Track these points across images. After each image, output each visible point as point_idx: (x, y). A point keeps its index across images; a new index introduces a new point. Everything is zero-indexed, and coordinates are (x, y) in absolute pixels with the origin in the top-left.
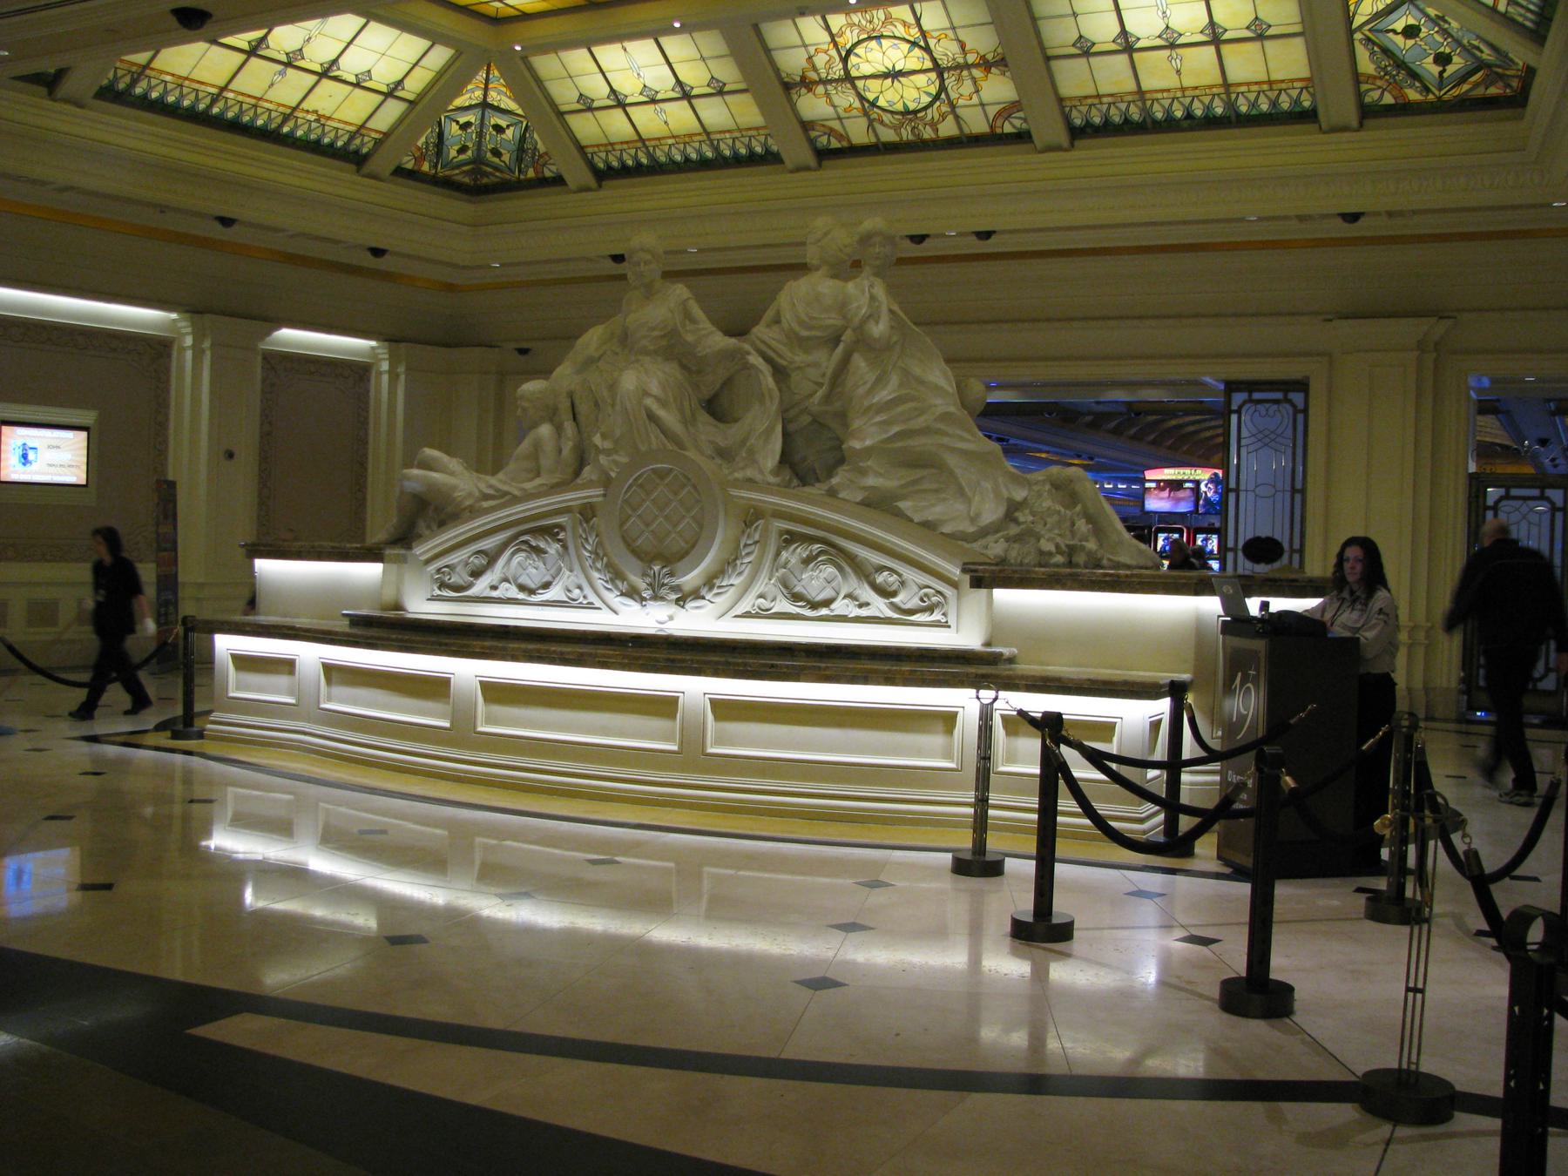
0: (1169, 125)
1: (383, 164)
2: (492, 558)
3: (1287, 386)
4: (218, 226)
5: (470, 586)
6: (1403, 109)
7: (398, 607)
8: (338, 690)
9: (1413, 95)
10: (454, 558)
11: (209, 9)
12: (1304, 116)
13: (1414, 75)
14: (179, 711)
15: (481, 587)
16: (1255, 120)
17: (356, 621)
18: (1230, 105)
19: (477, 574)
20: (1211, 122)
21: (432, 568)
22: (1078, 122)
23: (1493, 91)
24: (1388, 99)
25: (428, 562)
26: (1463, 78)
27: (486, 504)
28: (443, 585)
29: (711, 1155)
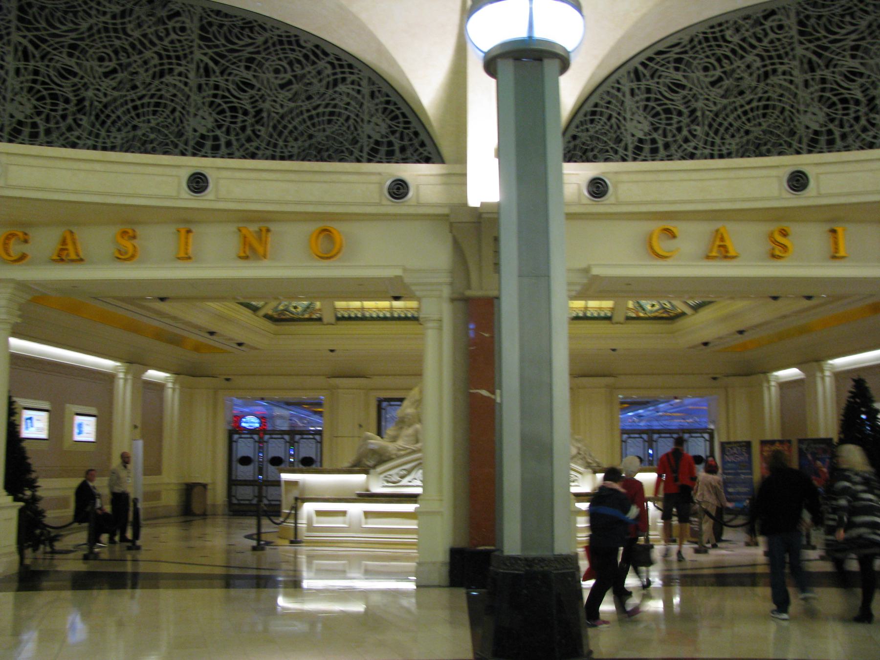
0: (372, 319)
1: (619, 317)
2: (409, 472)
3: (380, 409)
4: (208, 335)
5: (399, 481)
6: (638, 318)
7: (368, 490)
8: (370, 520)
9: (641, 315)
10: (392, 472)
11: (677, 234)
12: (608, 318)
13: (644, 309)
14: (254, 531)
15: (405, 482)
16: (593, 318)
17: (360, 495)
18: (585, 314)
19: (403, 477)
20: (385, 319)
21: (382, 476)
22: (339, 315)
23: (664, 315)
24: (634, 315)
25: (381, 473)
26: (656, 311)
27: (402, 453)
28: (388, 482)
29: (645, 657)
